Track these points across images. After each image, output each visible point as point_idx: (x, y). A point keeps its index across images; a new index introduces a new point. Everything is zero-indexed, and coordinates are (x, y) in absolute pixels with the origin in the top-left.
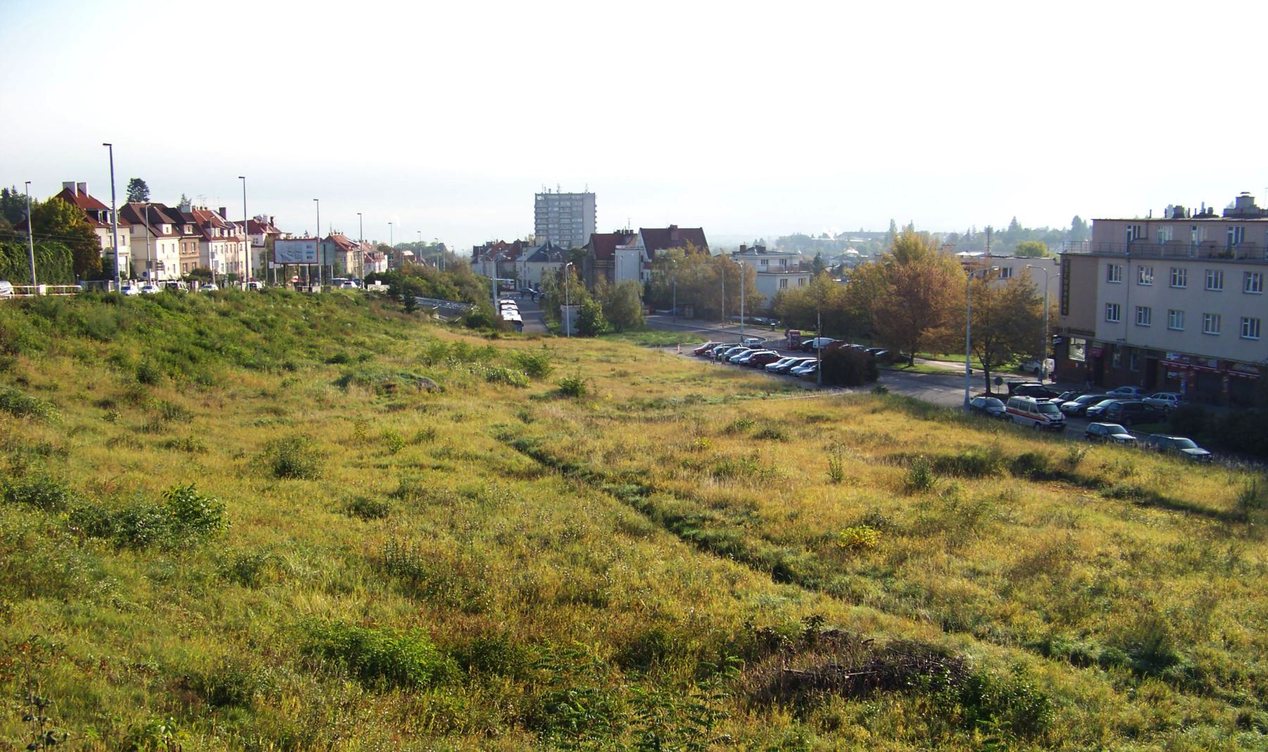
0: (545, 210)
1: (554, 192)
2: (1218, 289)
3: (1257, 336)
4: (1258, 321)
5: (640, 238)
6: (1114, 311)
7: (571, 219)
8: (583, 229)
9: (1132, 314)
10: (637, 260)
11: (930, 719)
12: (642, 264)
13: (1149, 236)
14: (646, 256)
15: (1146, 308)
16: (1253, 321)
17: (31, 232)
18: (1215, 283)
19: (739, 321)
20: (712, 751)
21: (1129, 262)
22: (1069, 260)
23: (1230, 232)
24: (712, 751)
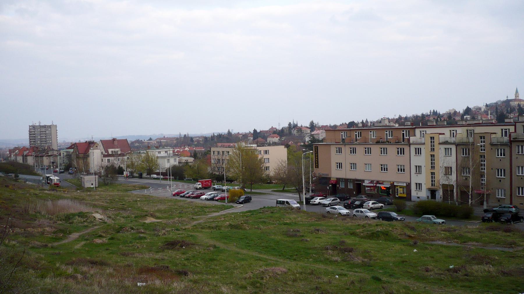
0: (33, 133)
1: (37, 124)
2: (385, 155)
3: (356, 169)
4: (341, 163)
5: (101, 144)
6: (340, 165)
7: (46, 136)
8: (51, 140)
9: (349, 166)
10: (100, 153)
11: (415, 248)
12: (102, 155)
13: (351, 136)
14: (104, 152)
15: (354, 164)
16: (339, 163)
17: (310, 174)
18: (354, 151)
19: (52, 174)
20: (0, 290)
21: (345, 146)
22: (317, 147)
23: (403, 132)
24: (0, 290)
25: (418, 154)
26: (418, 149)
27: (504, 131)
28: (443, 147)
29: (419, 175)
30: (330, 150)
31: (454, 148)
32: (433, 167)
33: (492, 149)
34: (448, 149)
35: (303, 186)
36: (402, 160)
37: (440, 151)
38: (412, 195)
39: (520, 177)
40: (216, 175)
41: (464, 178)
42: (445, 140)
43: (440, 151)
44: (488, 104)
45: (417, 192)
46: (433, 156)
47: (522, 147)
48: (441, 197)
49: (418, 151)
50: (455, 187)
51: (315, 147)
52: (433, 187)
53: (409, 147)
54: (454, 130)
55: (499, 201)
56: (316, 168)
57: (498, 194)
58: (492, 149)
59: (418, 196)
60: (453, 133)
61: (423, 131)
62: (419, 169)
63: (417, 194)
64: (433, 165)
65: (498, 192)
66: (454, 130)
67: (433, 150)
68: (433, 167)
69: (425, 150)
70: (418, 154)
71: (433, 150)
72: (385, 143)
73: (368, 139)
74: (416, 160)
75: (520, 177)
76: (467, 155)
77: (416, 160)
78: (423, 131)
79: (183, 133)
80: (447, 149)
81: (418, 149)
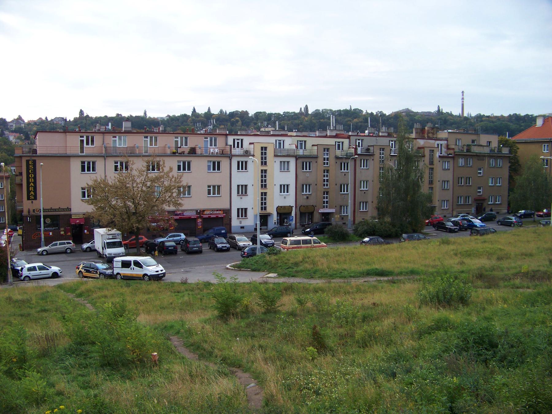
16: (214, 187)
25: (242, 169)
26: (242, 162)
27: (278, 142)
28: (278, 160)
29: (243, 197)
30: (70, 163)
31: (292, 162)
32: (264, 186)
33: (336, 163)
34: (284, 162)
35: (41, 237)
36: (216, 178)
37: (274, 165)
38: (232, 225)
39: (363, 192)
40: (85, 242)
41: (305, 197)
42: (71, 152)
43: (274, 165)
44: (197, 111)
45: (241, 220)
46: (264, 172)
47: (367, 160)
48: (275, 223)
49: (242, 166)
50: (294, 209)
51: (28, 161)
52: (264, 212)
53: (104, 160)
54: (239, 139)
55: (343, 219)
56: (29, 199)
57: (344, 211)
58: (336, 163)
59: (242, 225)
60: (238, 143)
61: (238, 139)
62: (243, 190)
63: (241, 222)
64: (264, 183)
65: (344, 209)
66: (239, 139)
67: (264, 163)
68: (264, 186)
69: (254, 164)
70: (242, 169)
71: (264, 163)
72: (182, 155)
73: (141, 148)
74: (239, 178)
75: (363, 192)
76: (156, 170)
77: (239, 178)
78: (359, 140)
79: (183, 113)
80: (286, 163)
81: (242, 162)
